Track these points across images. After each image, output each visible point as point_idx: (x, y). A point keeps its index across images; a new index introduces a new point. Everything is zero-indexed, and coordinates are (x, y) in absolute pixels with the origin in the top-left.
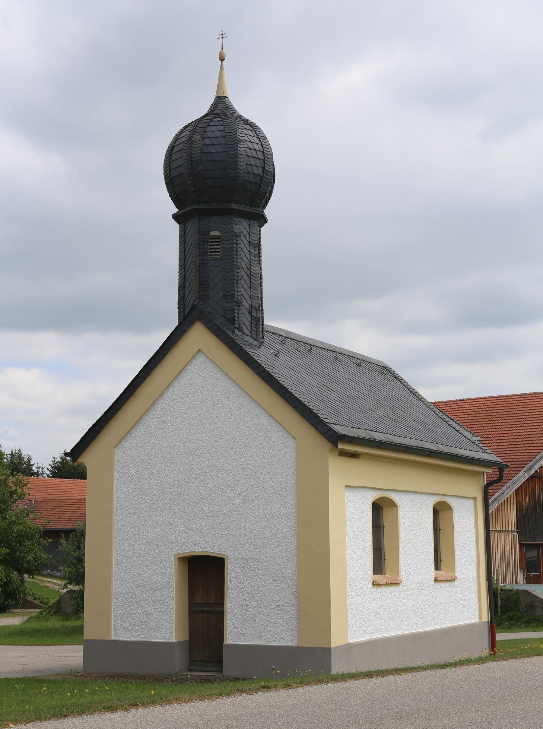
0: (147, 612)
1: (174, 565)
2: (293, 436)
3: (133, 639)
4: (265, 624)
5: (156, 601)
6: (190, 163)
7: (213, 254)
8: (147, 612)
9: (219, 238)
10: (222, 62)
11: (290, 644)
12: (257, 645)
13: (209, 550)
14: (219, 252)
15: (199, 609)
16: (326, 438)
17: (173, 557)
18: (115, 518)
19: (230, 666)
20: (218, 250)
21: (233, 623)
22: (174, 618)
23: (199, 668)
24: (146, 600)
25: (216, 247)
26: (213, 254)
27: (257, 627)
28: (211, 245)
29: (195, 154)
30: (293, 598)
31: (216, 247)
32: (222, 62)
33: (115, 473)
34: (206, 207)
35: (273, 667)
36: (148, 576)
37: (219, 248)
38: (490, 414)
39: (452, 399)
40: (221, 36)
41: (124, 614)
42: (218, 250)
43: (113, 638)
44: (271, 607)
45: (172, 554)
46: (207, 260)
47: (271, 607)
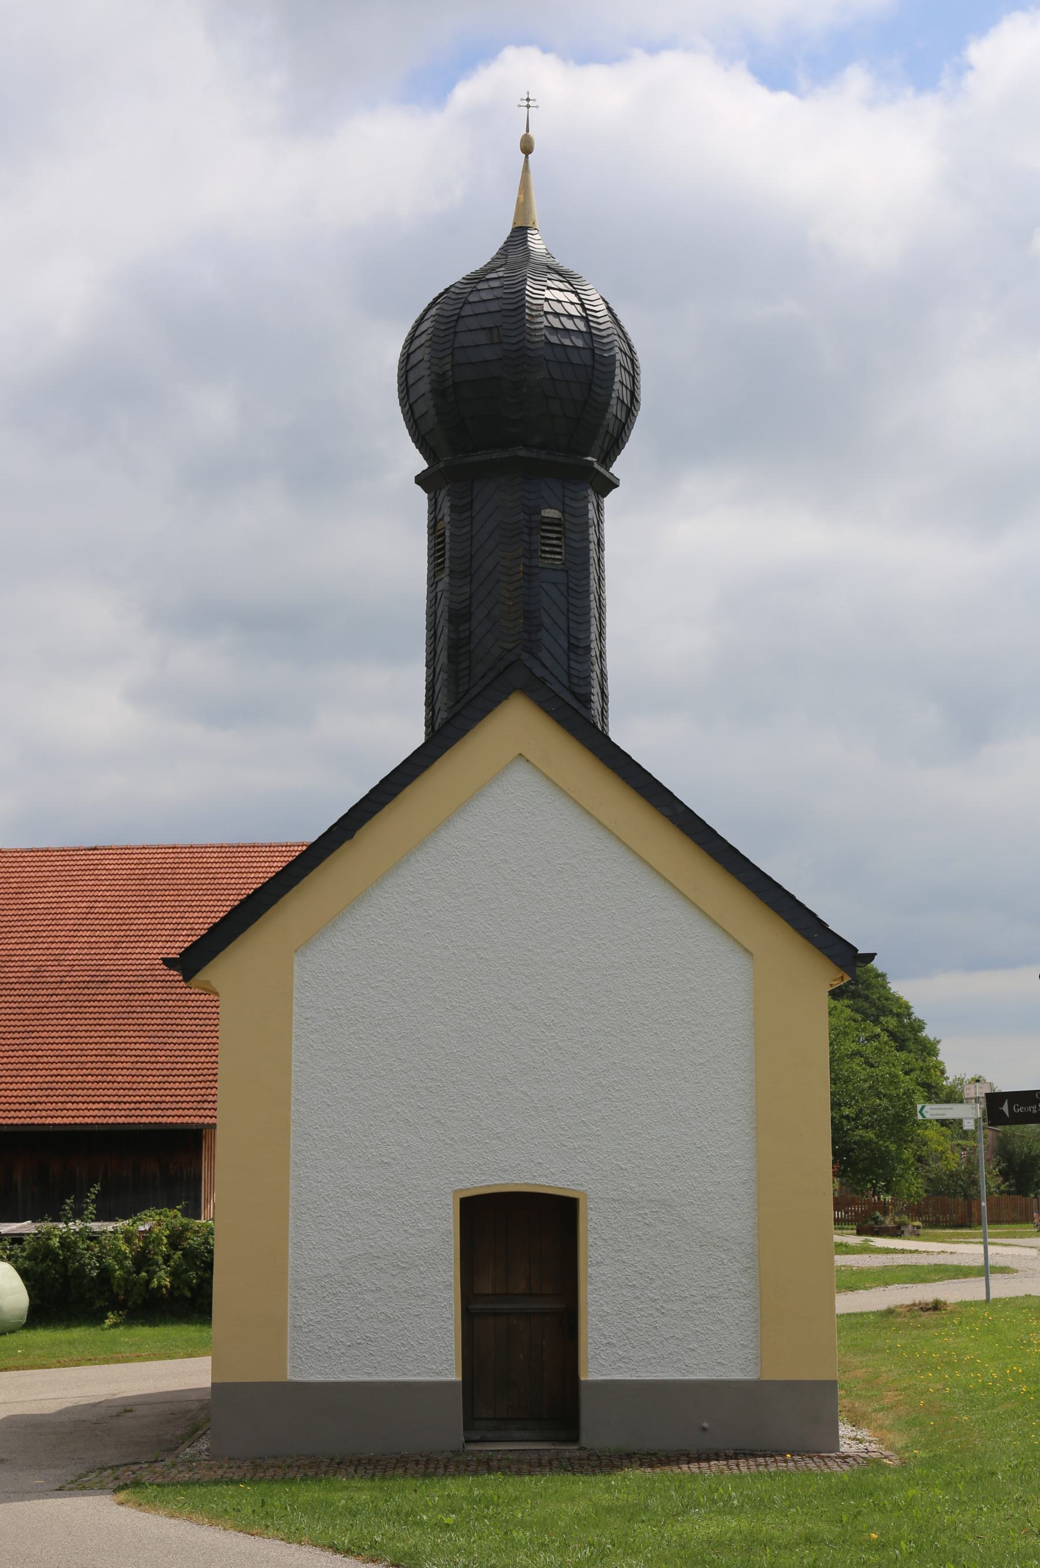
0: (382, 1317)
1: (451, 1212)
2: (746, 950)
3: (344, 1378)
4: (681, 1336)
5: (406, 1291)
6: (449, 351)
7: (548, 556)
8: (382, 1317)
9: (559, 525)
10: (527, 157)
11: (739, 1376)
12: (665, 1382)
13: (542, 1181)
14: (560, 553)
15: (490, 1306)
16: (830, 957)
17: (450, 1197)
18: (293, 1108)
19: (596, 1428)
20: (558, 550)
21: (603, 1335)
22: (452, 1328)
23: (489, 1435)
24: (379, 1290)
25: (554, 542)
26: (548, 556)
27: (661, 1342)
28: (543, 538)
29: (533, 343)
30: (744, 1281)
31: (554, 542)
32: (527, 157)
33: (295, 1009)
34: (543, 455)
35: (706, 1425)
36: (383, 1238)
37: (560, 547)
38: (171, 882)
39: (53, 845)
40: (526, 103)
41: (319, 1322)
42: (558, 550)
43: (292, 1376)
44: (693, 1299)
45: (448, 1190)
46: (537, 566)
47: (693, 1299)
